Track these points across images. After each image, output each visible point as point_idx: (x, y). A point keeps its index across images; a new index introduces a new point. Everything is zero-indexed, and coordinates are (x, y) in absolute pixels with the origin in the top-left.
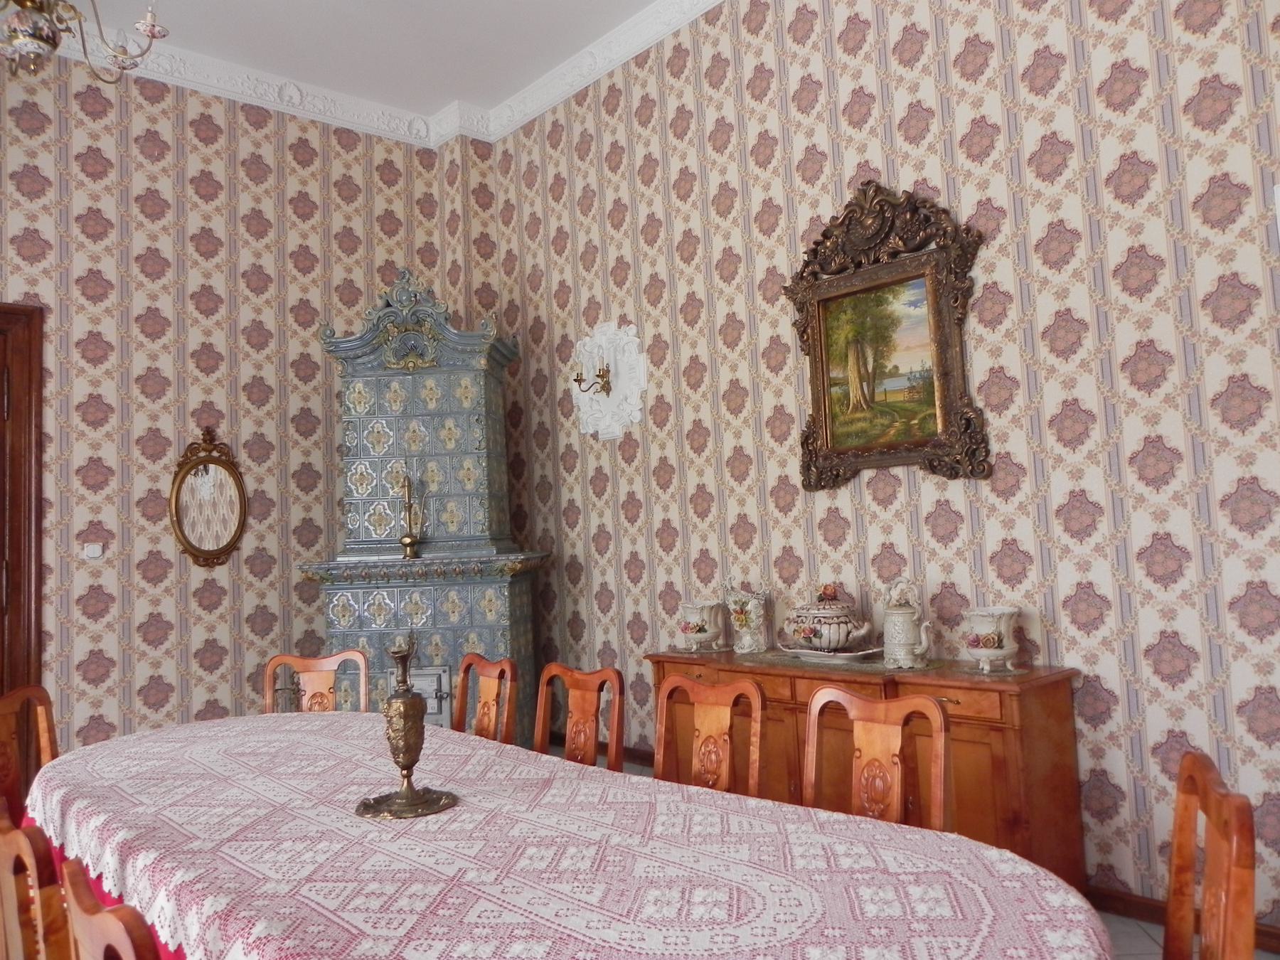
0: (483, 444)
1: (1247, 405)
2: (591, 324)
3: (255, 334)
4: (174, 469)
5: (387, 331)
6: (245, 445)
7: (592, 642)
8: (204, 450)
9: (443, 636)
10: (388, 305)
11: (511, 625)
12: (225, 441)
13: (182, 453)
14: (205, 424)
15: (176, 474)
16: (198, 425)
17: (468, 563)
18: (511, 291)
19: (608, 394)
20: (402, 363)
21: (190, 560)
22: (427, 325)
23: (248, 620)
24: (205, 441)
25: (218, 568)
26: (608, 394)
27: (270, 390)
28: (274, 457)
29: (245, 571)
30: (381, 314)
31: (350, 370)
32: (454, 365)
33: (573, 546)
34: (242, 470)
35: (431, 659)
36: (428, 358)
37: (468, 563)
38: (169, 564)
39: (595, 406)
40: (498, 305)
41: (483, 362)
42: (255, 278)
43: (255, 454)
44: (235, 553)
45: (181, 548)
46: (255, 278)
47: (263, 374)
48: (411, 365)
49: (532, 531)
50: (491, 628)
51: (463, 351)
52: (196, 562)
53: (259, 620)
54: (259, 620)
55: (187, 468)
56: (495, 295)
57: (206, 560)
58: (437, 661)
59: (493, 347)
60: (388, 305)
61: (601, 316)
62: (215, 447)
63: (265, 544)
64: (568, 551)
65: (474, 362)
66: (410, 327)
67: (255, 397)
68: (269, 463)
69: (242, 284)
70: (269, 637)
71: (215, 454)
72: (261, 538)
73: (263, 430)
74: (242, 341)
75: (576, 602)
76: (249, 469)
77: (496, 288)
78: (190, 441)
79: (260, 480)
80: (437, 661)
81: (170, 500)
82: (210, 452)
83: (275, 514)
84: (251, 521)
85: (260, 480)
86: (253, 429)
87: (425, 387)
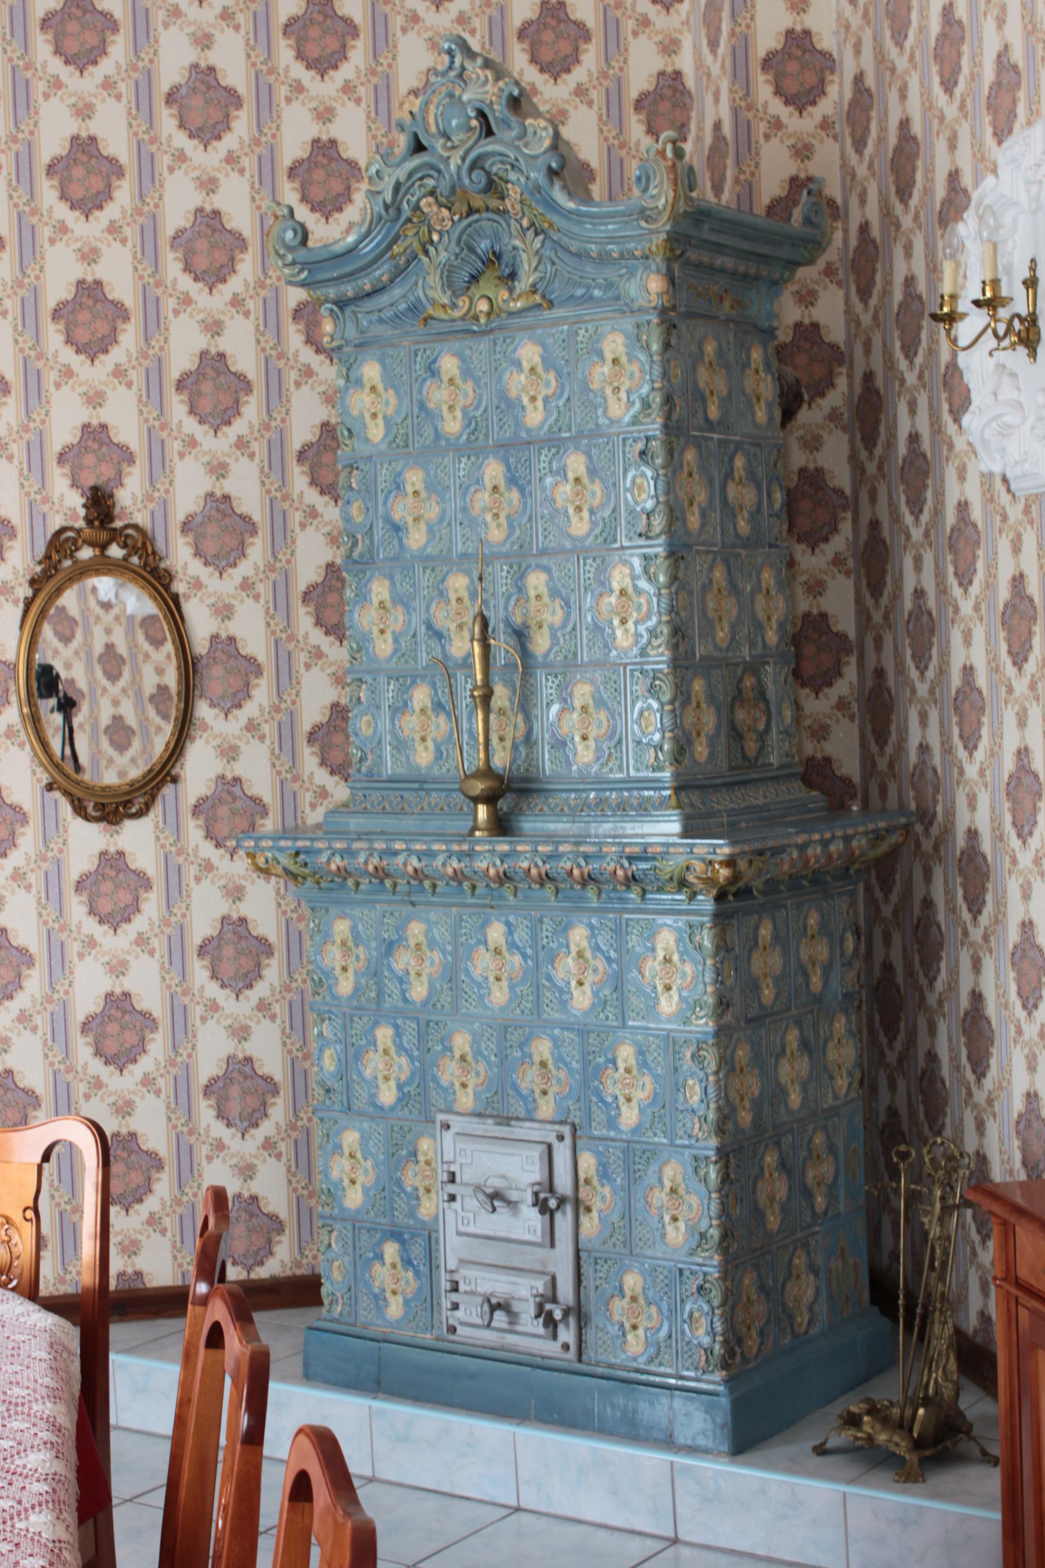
0: (658, 523)
1: (133, 1175)
2: (1001, 135)
3: (202, 245)
4: (24, 591)
5: (424, 218)
6: (186, 526)
7: (1004, 1085)
8: (92, 544)
9: (557, 1043)
10: (419, 147)
11: (717, 1034)
12: (140, 518)
13: (41, 551)
14: (89, 480)
15: (28, 604)
16: (74, 484)
17: (600, 856)
18: (857, 50)
19: (1033, 353)
20: (463, 303)
21: (65, 807)
22: (514, 193)
23: (202, 950)
24: (89, 522)
25: (129, 825)
26: (1033, 353)
27: (244, 383)
28: (257, 551)
29: (194, 832)
30: (401, 174)
31: (351, 332)
32: (590, 298)
33: (972, 802)
34: (179, 587)
35: (530, 1103)
36: (523, 284)
37: (600, 856)
38: (20, 814)
39: (1007, 392)
40: (832, 90)
41: (656, 284)
42: (197, 101)
43: (210, 547)
44: (168, 790)
45: (45, 779)
46: (197, 101)
47: (224, 344)
48: (483, 306)
49: (901, 747)
50: (670, 1041)
51: (604, 259)
52: (79, 809)
53: (228, 951)
54: (228, 951)
55: (49, 587)
56: (827, 62)
57: (100, 806)
58: (546, 1109)
59: (675, 240)
60: (419, 147)
61: (1021, 110)
62: (115, 535)
63: (239, 769)
64: (963, 821)
65: (632, 288)
66: (478, 202)
67: (206, 404)
68: (245, 569)
69: (167, 121)
70: (254, 995)
71: (115, 551)
72: (230, 753)
73: (229, 486)
74: (173, 266)
75: (977, 965)
76: (197, 584)
77: (826, 40)
78: (56, 522)
79: (224, 612)
80: (546, 1109)
81: (16, 666)
82: (104, 547)
83: (262, 693)
84: (203, 710)
85: (224, 612)
86: (205, 484)
87: (518, 364)
